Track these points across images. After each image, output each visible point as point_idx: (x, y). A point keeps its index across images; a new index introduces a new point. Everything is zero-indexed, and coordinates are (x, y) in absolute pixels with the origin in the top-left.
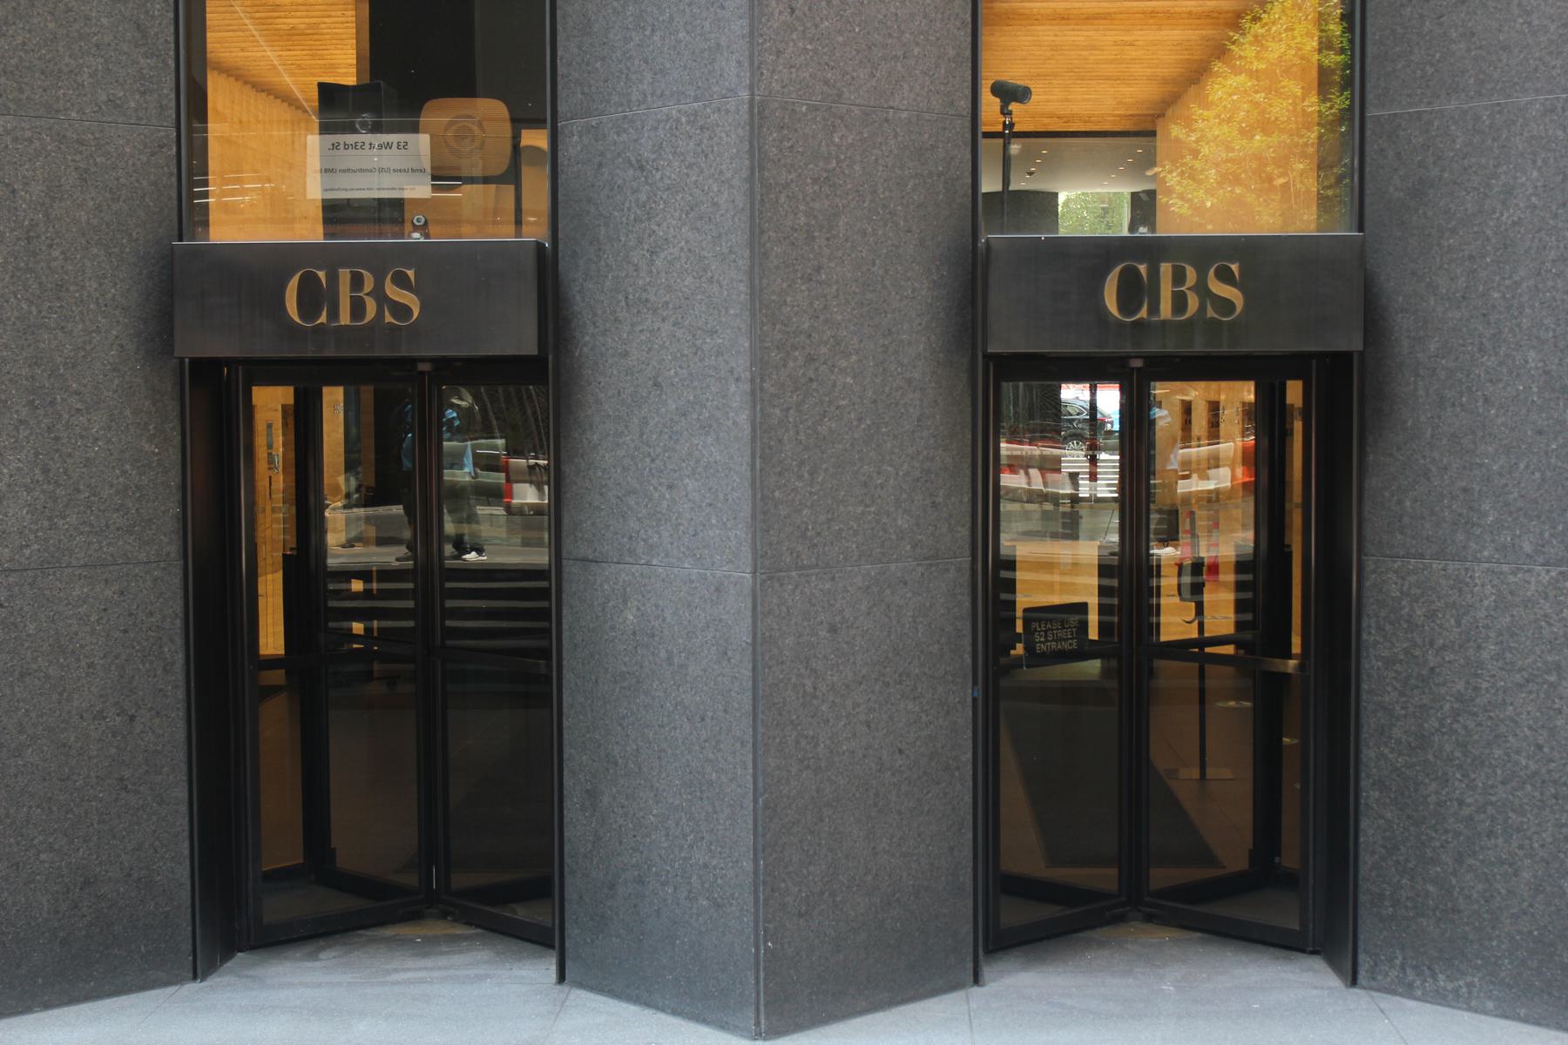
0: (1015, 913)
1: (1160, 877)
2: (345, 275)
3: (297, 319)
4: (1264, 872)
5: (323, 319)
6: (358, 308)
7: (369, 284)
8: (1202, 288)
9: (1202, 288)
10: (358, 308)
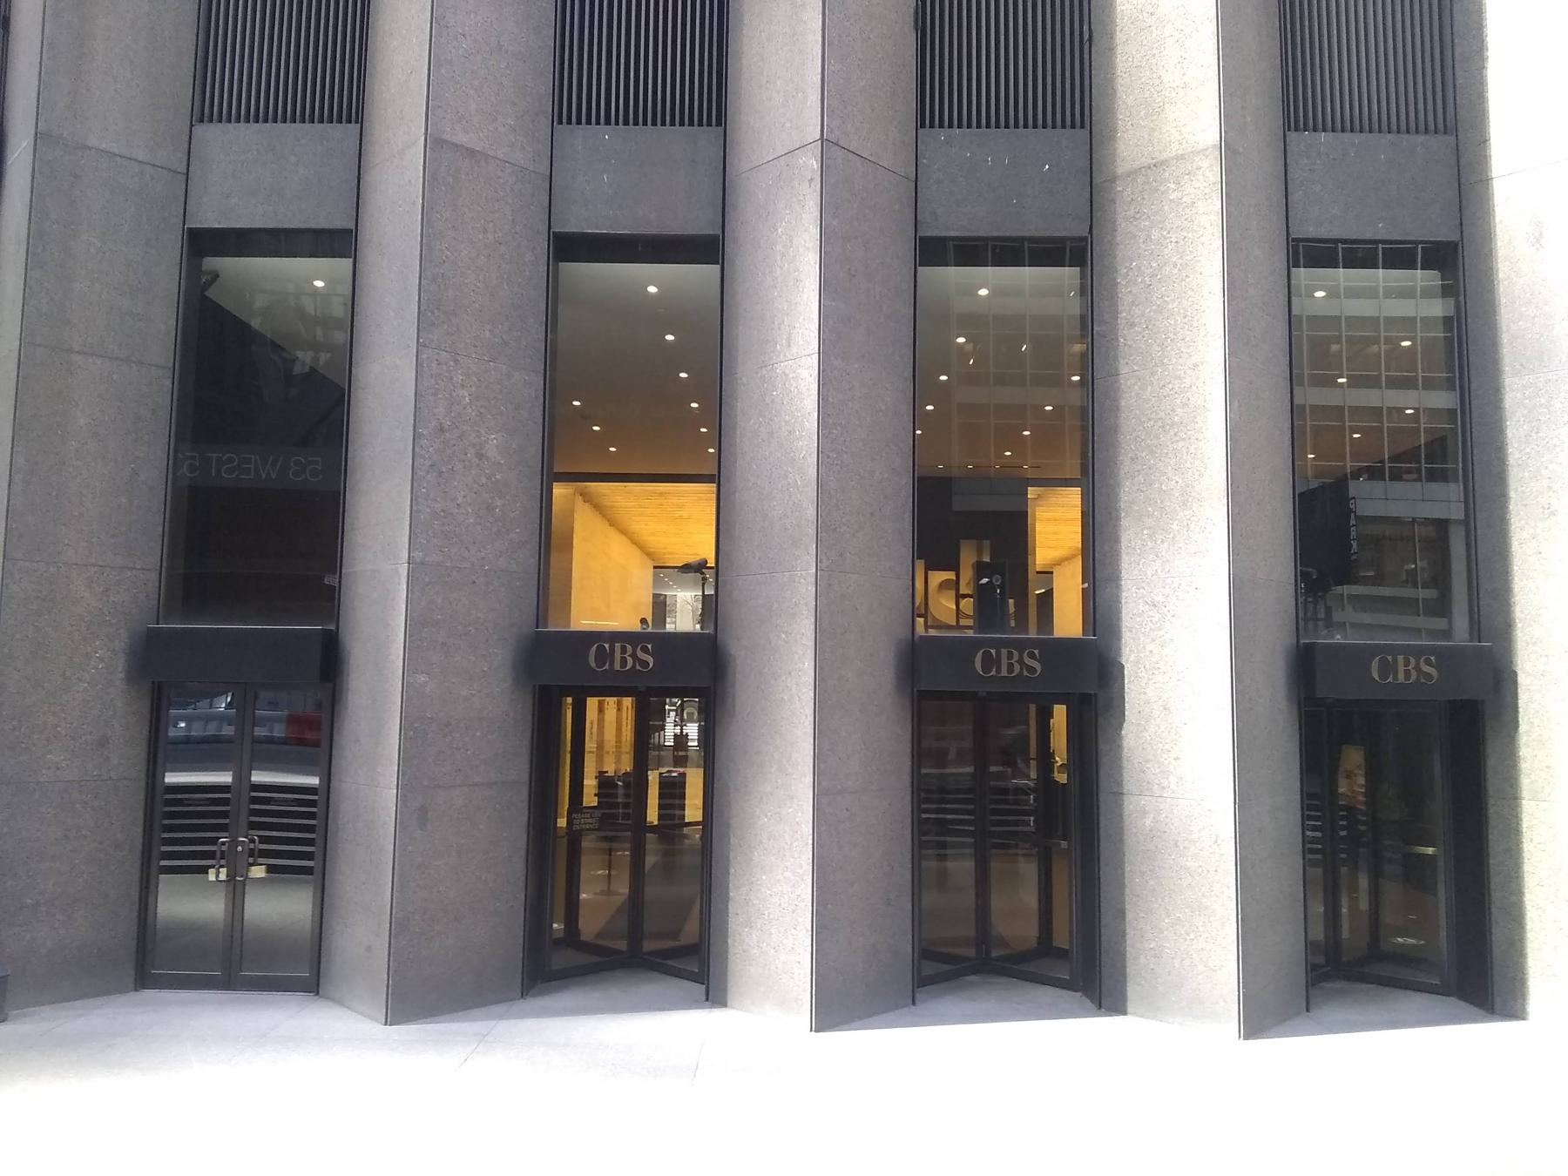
0: (930, 968)
1: (649, 946)
2: (1004, 652)
3: (593, 665)
4: (1045, 948)
5: (993, 673)
6: (1010, 668)
7: (1412, 661)
8: (634, 655)
9: (1021, 661)
10: (1010, 668)
